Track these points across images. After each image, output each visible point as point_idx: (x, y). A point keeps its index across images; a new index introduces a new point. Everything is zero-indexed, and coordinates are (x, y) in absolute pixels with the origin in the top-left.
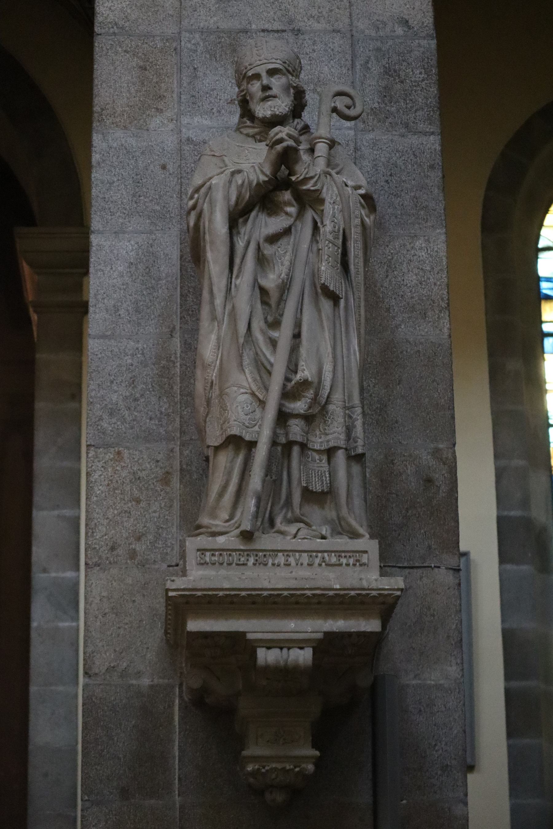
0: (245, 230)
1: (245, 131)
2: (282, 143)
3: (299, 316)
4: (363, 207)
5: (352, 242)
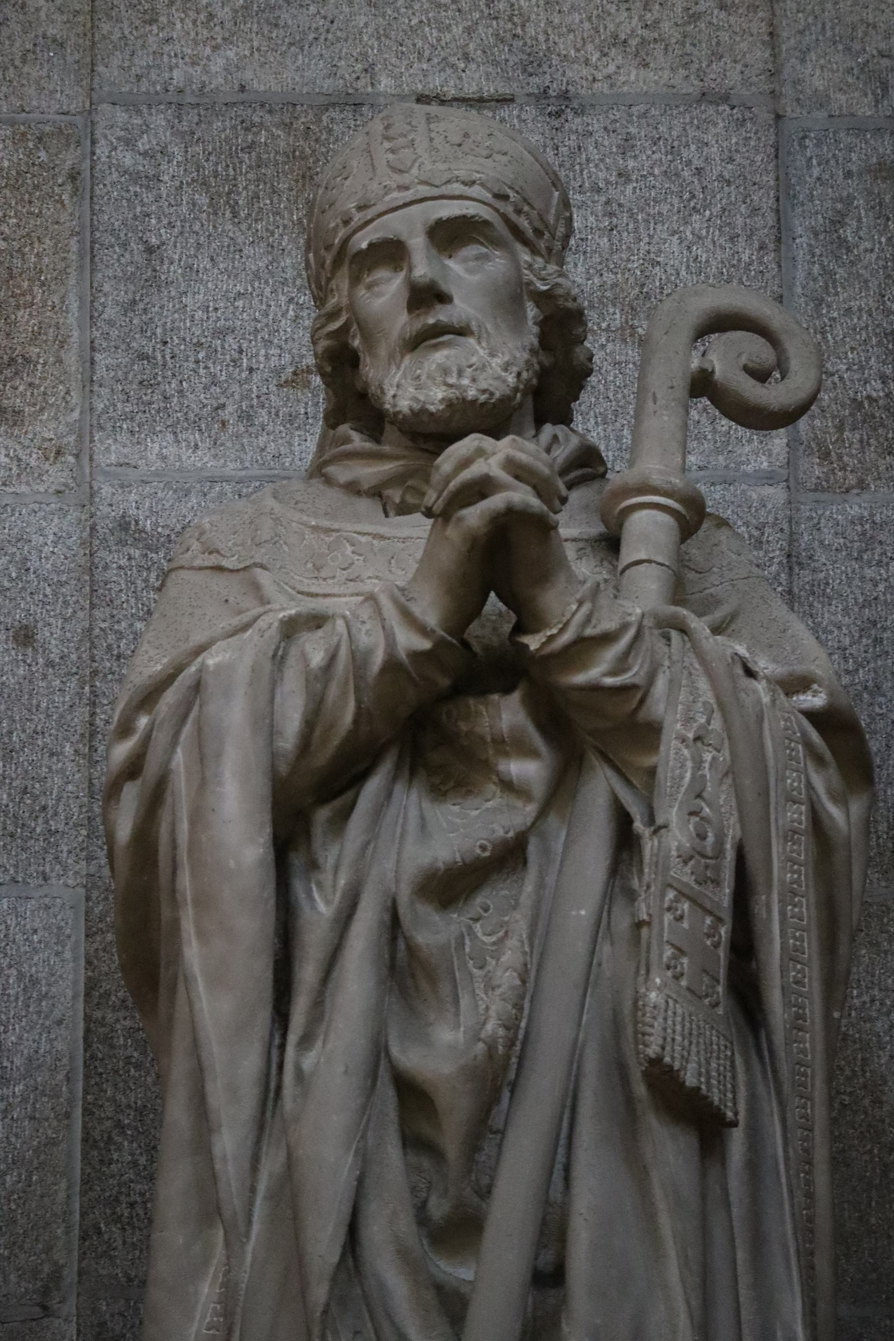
0: (337, 857)
1: (342, 473)
2: (483, 496)
3: (556, 1194)
4: (819, 760)
5: (775, 897)
